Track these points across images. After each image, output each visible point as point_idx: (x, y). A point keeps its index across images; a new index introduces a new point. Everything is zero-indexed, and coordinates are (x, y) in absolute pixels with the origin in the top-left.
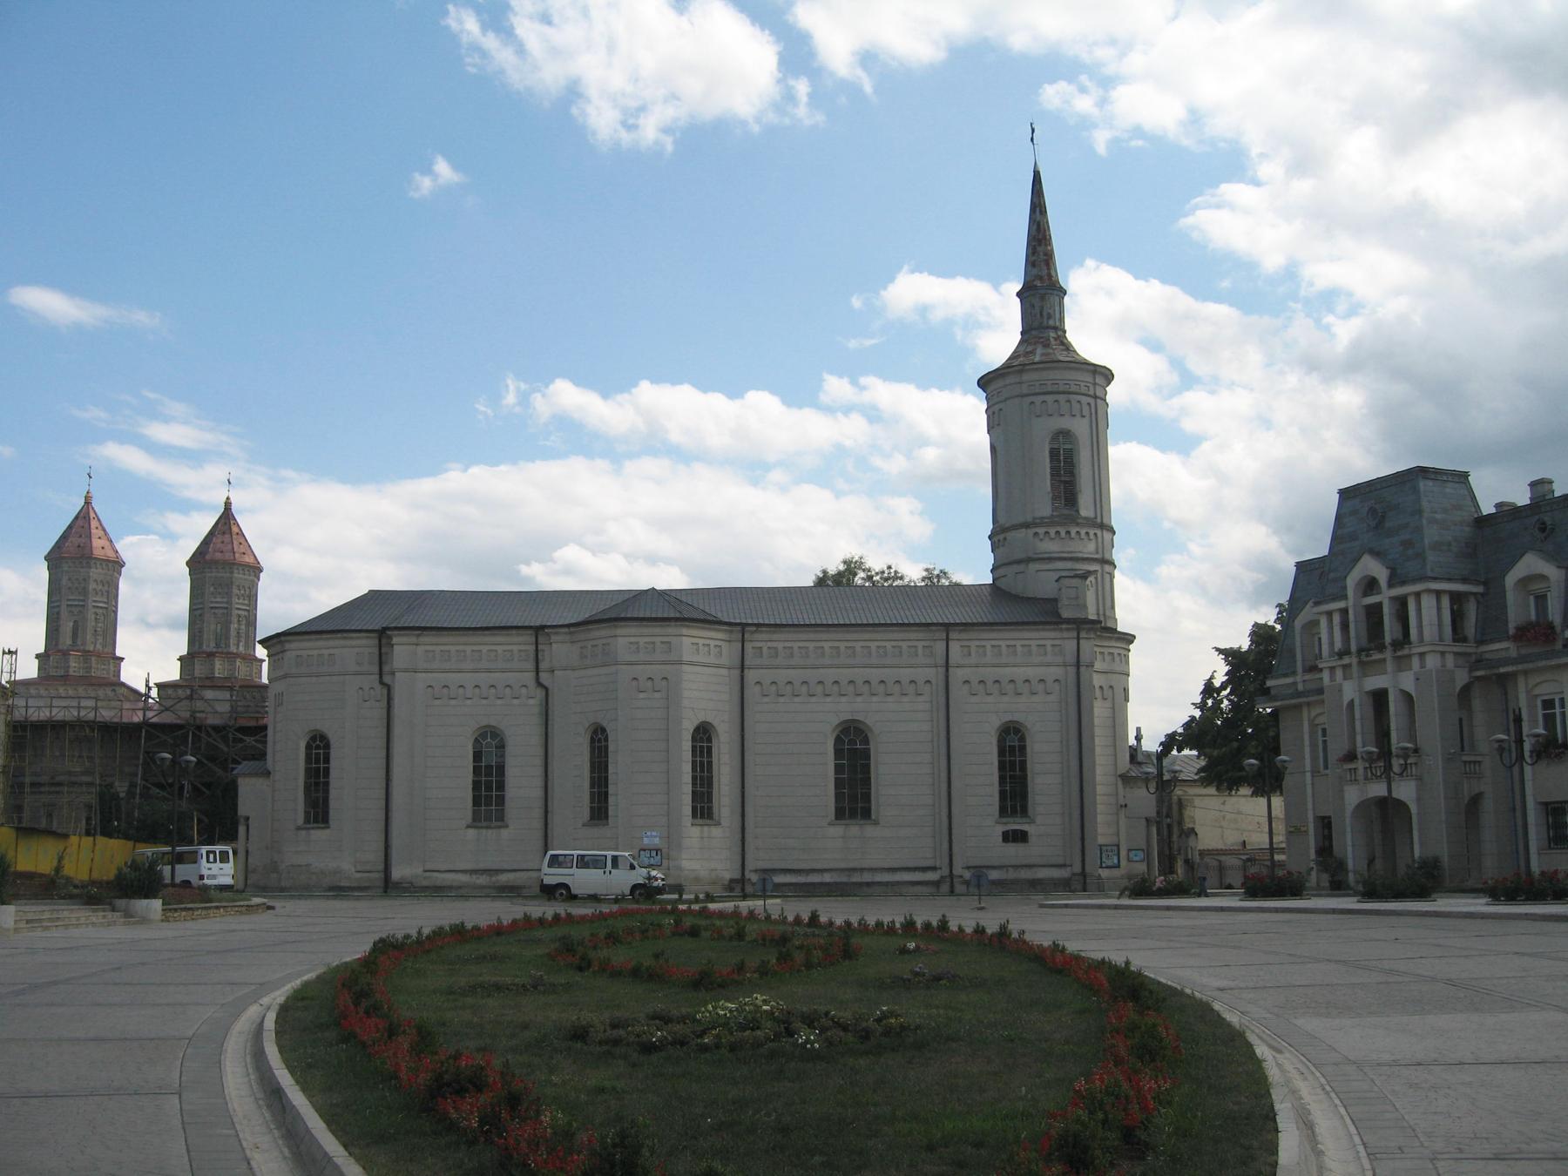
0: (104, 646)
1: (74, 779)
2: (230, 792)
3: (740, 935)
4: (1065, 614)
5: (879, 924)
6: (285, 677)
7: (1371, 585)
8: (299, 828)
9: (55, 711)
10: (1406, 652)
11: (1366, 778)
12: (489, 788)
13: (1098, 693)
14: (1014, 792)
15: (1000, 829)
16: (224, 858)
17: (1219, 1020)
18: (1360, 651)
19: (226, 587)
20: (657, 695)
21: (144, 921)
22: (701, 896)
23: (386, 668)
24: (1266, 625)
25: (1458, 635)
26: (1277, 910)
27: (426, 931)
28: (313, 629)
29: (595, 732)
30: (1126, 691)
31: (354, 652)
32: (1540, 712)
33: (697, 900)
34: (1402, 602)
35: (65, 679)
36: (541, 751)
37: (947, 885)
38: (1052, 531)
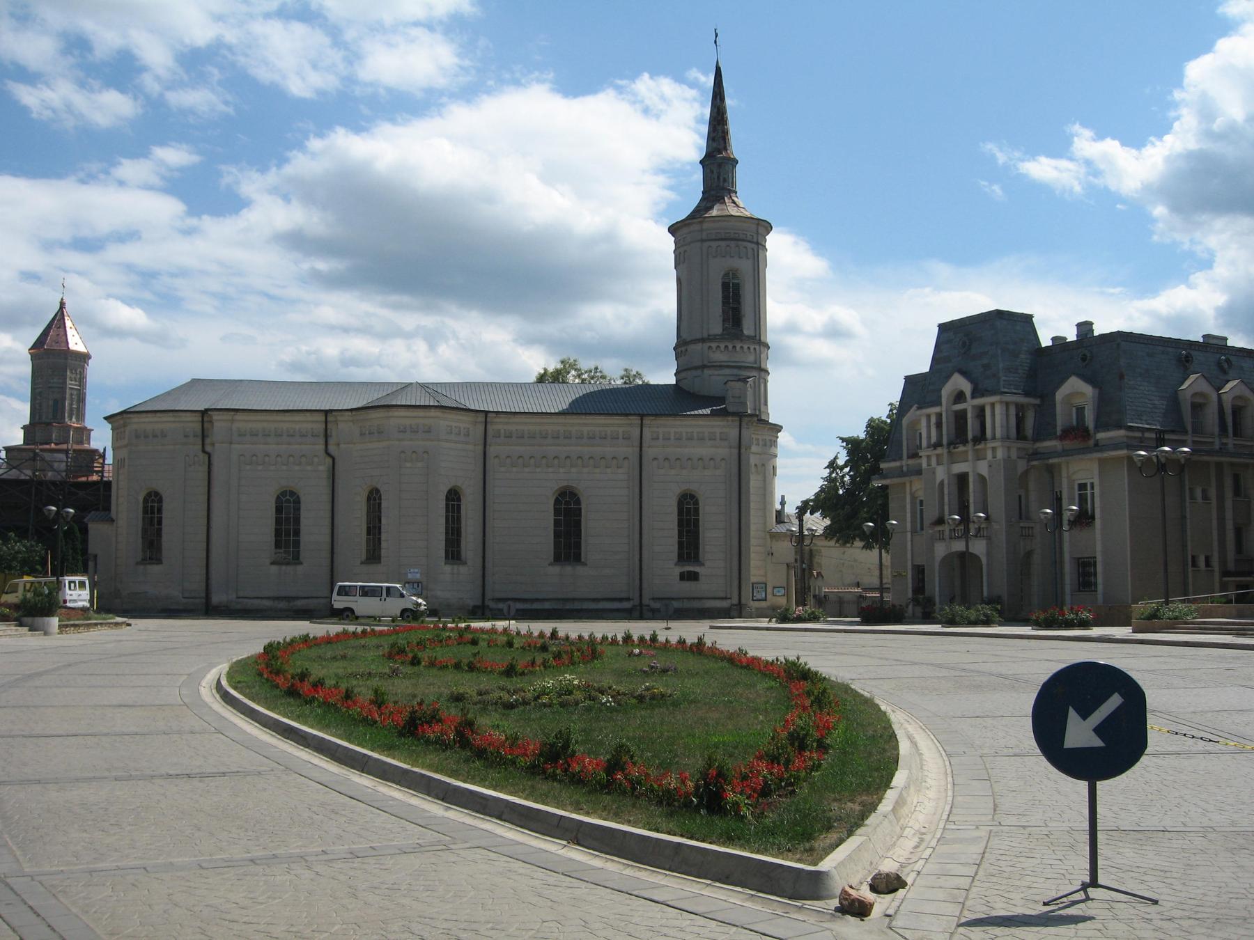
3: (510, 644)
7: (960, 397)
8: (137, 564)
12: (288, 534)
13: (753, 469)
15: (678, 570)
16: (82, 584)
17: (855, 694)
18: (949, 444)
20: (420, 464)
25: (1021, 435)
27: (288, 640)
29: (371, 492)
32: (1077, 493)
34: (981, 412)
36: (328, 507)
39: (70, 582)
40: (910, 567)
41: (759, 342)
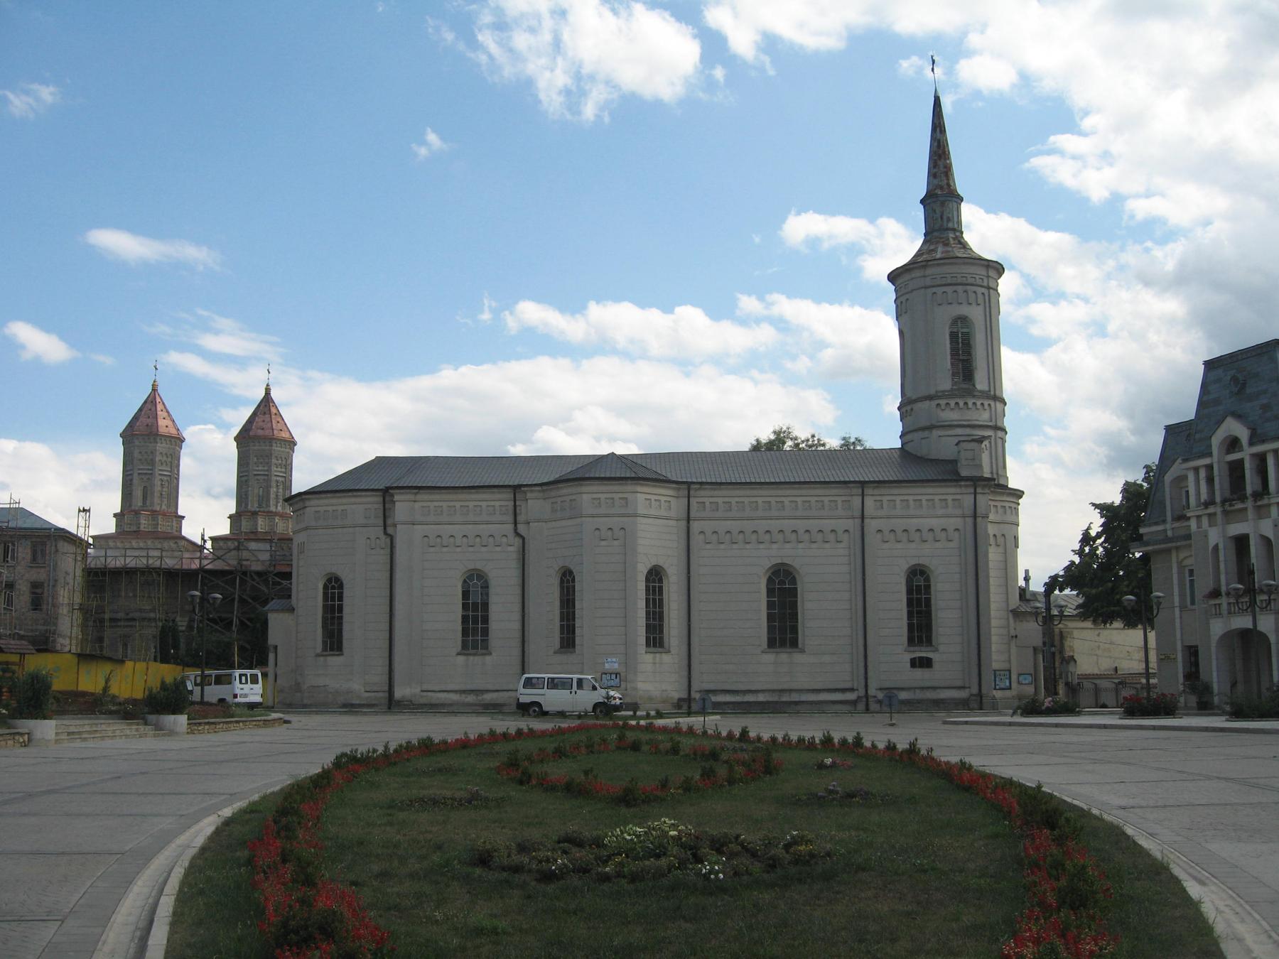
0: (169, 506)
1: (144, 615)
2: (262, 627)
3: (675, 750)
4: (964, 473)
5: (801, 740)
6: (306, 528)
7: (1233, 444)
8: (318, 655)
9: (128, 560)
10: (1265, 501)
11: (1230, 613)
13: (992, 540)
14: (920, 624)
15: (908, 657)
16: (254, 680)
18: (1224, 501)
19: (266, 458)
20: (616, 543)
21: (172, 733)
22: (653, 713)
23: (389, 522)
24: (1135, 484)
26: (1154, 728)
27: (392, 748)
28: (329, 488)
29: (564, 575)
30: (1016, 538)
31: (362, 509)
33: (648, 716)
34: (1261, 459)
35: (137, 533)
37: (863, 704)
38: (952, 403)
39: (241, 676)
40: (1179, 647)
41: (995, 398)
